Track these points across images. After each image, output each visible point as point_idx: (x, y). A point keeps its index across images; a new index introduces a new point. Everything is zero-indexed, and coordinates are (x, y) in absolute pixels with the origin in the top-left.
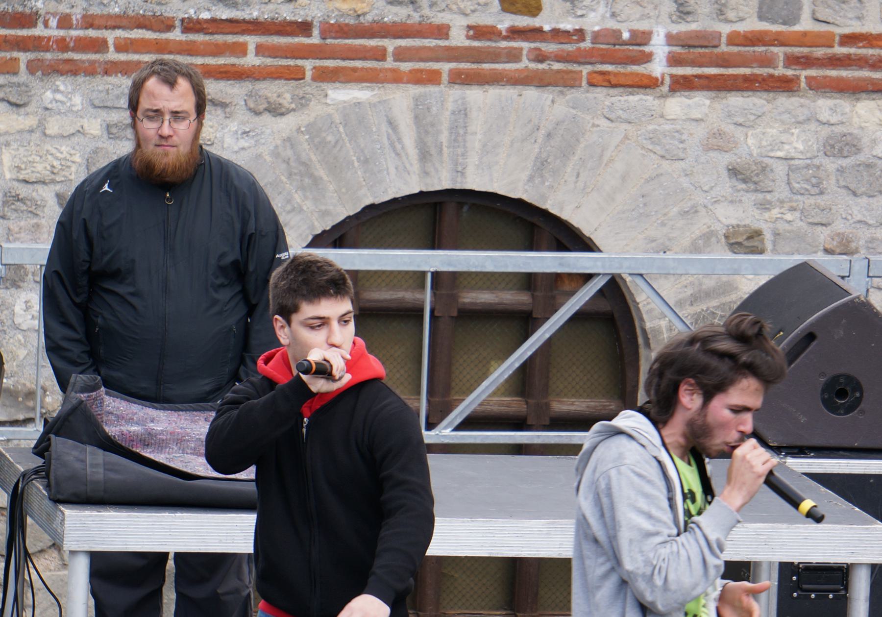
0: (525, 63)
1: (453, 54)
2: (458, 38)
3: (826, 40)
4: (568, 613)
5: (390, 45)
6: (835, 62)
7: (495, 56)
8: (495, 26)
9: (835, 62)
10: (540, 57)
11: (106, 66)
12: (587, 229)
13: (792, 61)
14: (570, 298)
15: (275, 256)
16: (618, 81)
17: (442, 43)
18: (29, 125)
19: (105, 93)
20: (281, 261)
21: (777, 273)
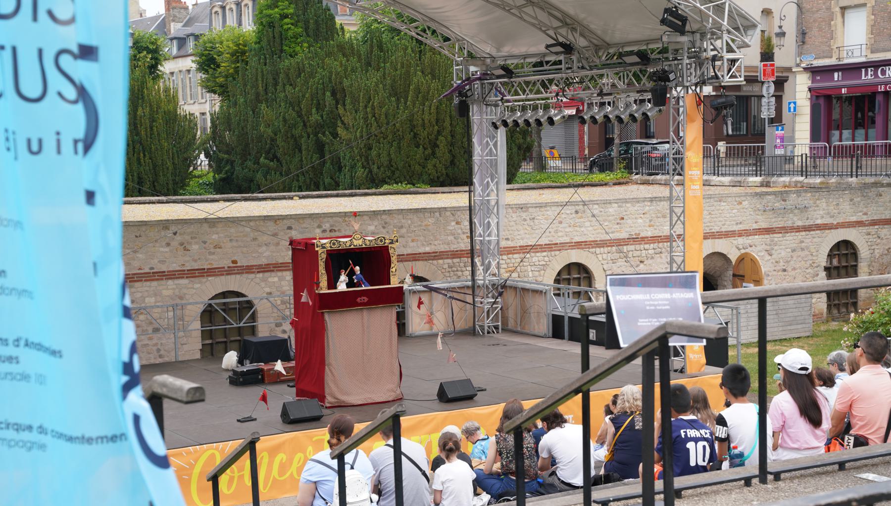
0: (236, 271)
1: (226, 271)
2: (226, 268)
3: (277, 264)
4: (201, 398)
5: (217, 270)
6: (279, 267)
7: (232, 270)
8: (201, 350)
9: (279, 267)
10: (238, 270)
11: (402, 33)
12: (243, 292)
13: (273, 267)
14: (682, 288)
15: (663, 462)
16: (450, 248)
17: (758, 288)
18: (288, 243)
19: (554, 151)
20: (659, 462)
21: (424, 277)
